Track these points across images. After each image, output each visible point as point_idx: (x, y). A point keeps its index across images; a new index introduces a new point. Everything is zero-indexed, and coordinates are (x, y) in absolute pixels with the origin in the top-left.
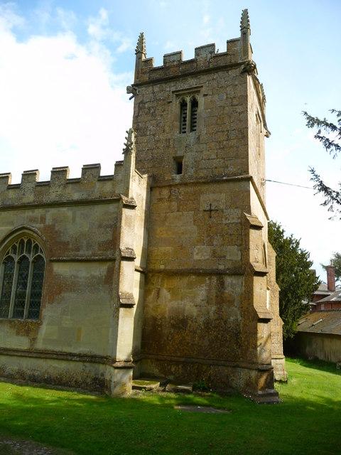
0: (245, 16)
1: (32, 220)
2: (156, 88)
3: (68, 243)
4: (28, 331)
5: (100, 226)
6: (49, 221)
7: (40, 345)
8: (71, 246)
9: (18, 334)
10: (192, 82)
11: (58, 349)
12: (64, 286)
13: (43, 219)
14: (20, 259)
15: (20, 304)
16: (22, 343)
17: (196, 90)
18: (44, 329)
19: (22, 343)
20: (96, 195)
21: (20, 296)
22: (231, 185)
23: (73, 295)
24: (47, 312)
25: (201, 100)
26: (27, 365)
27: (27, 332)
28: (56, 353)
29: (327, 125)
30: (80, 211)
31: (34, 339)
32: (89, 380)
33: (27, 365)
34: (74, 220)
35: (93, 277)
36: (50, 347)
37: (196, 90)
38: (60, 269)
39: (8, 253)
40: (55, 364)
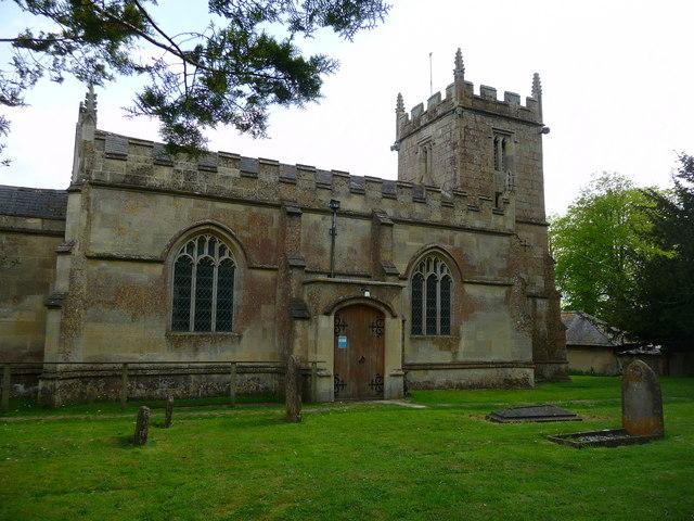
0: (536, 78)
1: (442, 240)
2: (478, 118)
3: (474, 267)
4: (451, 346)
5: (497, 255)
6: (457, 244)
7: (461, 358)
8: (477, 270)
9: (441, 349)
10: (504, 125)
11: (475, 359)
12: (471, 308)
13: (452, 241)
14: (201, 261)
15: (431, 322)
16: (445, 357)
17: (507, 134)
18: (463, 344)
19: (445, 357)
20: (491, 227)
21: (432, 313)
22: (537, 227)
23: (483, 314)
24: (465, 329)
25: (510, 144)
26: (454, 376)
27: (449, 347)
28: (479, 363)
29: (148, 69)
30: (483, 238)
31: (456, 353)
32: (502, 382)
33: (454, 376)
34: (478, 246)
35: (497, 299)
36: (470, 359)
37: (507, 134)
38: (470, 290)
39: (182, 251)
40: (476, 372)
